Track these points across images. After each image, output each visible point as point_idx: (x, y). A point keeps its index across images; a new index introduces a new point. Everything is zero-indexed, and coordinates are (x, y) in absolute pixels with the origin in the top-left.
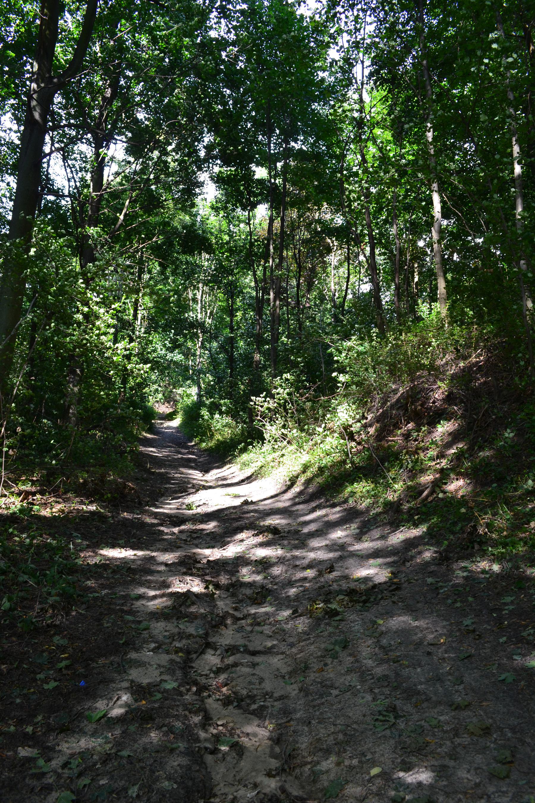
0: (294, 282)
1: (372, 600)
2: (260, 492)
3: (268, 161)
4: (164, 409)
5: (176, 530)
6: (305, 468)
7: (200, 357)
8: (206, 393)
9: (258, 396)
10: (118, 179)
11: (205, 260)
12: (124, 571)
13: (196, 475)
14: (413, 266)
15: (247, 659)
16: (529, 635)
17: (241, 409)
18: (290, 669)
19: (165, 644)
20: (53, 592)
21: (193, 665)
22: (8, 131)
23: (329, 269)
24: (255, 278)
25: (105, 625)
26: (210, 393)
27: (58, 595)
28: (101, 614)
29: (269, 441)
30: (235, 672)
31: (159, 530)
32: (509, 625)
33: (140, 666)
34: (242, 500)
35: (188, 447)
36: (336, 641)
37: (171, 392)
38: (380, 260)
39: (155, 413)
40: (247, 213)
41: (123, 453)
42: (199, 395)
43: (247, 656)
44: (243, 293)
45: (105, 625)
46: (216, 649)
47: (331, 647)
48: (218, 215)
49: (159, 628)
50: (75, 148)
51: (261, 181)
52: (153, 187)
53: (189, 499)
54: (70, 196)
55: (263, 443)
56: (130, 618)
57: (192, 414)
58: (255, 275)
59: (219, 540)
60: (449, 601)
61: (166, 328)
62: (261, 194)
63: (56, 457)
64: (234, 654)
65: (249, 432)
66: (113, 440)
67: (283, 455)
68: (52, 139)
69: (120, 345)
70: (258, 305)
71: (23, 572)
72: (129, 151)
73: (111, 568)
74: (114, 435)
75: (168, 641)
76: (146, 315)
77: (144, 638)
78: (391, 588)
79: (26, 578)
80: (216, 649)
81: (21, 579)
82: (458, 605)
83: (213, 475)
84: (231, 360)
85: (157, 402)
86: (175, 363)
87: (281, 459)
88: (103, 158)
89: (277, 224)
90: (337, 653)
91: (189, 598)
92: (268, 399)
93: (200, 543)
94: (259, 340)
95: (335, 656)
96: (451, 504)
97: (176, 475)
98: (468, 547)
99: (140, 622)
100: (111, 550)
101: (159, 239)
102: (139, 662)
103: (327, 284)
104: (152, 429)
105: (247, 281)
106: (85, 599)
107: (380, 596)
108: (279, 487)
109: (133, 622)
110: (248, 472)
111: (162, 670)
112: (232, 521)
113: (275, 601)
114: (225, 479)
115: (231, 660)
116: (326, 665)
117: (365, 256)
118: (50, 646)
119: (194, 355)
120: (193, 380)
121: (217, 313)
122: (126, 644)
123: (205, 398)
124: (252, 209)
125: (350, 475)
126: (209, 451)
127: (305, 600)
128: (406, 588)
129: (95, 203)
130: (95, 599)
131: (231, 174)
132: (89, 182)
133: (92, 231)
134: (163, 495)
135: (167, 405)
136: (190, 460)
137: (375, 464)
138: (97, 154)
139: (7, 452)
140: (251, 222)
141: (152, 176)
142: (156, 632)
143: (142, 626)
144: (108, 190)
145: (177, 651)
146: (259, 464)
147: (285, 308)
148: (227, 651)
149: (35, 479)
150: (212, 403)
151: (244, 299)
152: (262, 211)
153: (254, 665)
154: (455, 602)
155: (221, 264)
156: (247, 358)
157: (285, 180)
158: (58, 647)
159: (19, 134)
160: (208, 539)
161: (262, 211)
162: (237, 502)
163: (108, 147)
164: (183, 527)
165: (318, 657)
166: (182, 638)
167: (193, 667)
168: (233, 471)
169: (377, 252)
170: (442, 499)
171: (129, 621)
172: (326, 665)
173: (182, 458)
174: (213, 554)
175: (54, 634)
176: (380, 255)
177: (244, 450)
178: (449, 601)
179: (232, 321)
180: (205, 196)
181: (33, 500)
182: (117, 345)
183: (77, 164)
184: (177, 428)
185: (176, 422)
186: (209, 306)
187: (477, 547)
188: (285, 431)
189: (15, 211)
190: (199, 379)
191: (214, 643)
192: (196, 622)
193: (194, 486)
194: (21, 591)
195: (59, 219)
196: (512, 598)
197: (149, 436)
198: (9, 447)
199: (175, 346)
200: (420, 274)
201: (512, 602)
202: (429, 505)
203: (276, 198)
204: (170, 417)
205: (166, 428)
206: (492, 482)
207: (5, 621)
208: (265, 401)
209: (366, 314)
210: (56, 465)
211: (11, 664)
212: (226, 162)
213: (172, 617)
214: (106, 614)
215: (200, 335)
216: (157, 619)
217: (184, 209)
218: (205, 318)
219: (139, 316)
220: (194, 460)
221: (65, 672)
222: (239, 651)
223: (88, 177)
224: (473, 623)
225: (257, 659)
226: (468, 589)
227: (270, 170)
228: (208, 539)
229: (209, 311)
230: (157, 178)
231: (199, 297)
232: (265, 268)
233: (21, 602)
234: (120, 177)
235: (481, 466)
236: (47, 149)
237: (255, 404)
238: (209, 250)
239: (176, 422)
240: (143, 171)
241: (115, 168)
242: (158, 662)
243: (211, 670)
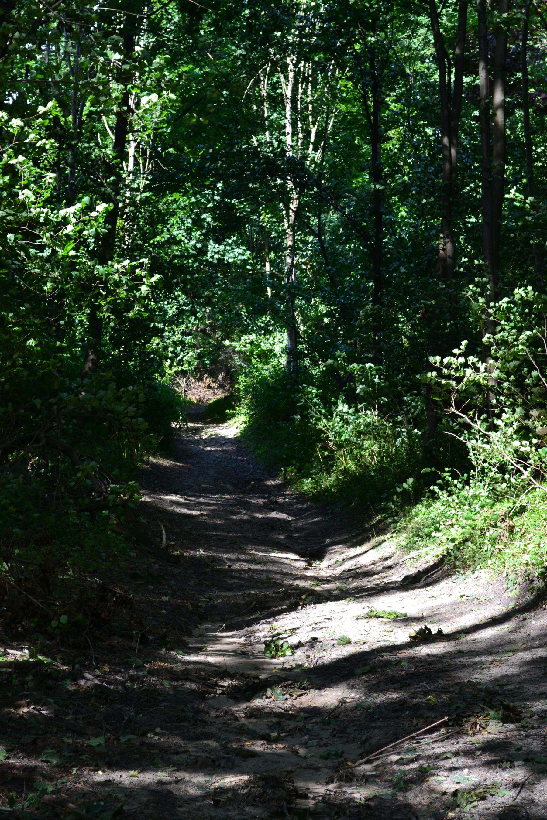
2: (471, 601)
4: (201, 391)
7: (293, 254)
8: (312, 347)
17: (405, 386)
24: (437, 36)
26: (321, 343)
37: (219, 347)
41: (94, 509)
42: (292, 352)
44: (406, 77)
53: (285, 622)
58: (434, 26)
61: (199, 177)
65: (426, 450)
67: (523, 509)
83: (334, 563)
85: (184, 373)
87: (517, 521)
92: (472, 359)
94: (451, 204)
97: (237, 566)
104: (170, 445)
105: (416, 43)
108: (513, 593)
110: (428, 555)
114: (369, 574)
119: (279, 248)
120: (276, 314)
121: (335, 133)
123: (307, 362)
126: (321, 500)
134: (203, 618)
135: (208, 381)
146: (457, 533)
147: (519, 113)
156: (419, 248)
162: (402, 635)
164: (258, 702)
168: (386, 552)
173: (252, 521)
177: (413, 498)
185: (232, 428)
186: (315, 113)
190: (291, 309)
197: (163, 462)
199: (228, 224)
204: (218, 413)
208: (466, 365)
218: (305, 146)
219: (131, 150)
228: (325, 734)
229: (314, 131)
237: (441, 375)
239: (232, 428)
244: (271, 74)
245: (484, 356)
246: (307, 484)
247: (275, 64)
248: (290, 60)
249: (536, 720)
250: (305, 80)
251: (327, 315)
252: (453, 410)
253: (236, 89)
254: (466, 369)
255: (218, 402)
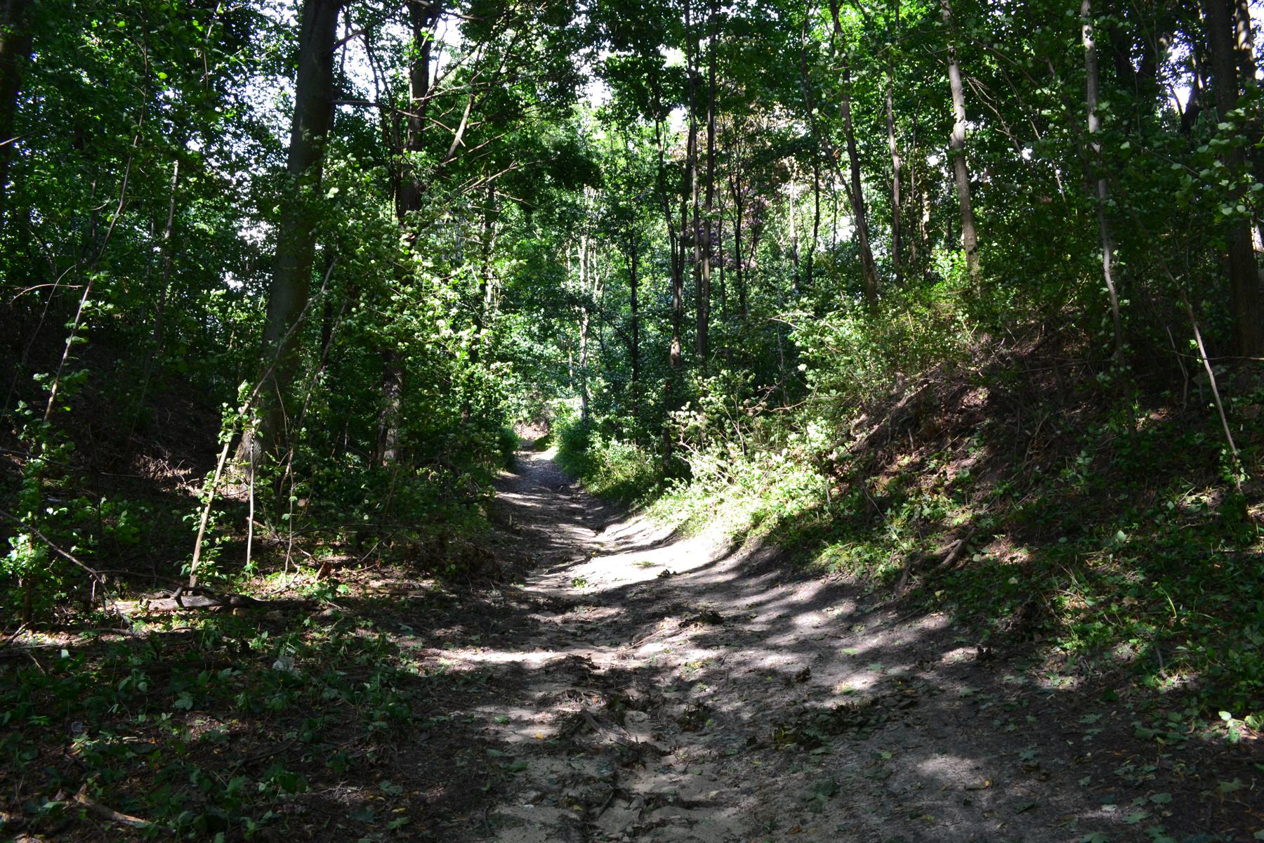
0: (729, 228)
1: (872, 721)
2: (681, 560)
3: (687, 38)
4: (530, 433)
5: (558, 619)
6: (757, 520)
8: (597, 406)
9: (677, 408)
10: (451, 77)
11: (589, 198)
12: (483, 682)
13: (585, 536)
14: (921, 197)
15: (679, 814)
16: (1126, 773)
17: (652, 429)
18: (747, 829)
19: (551, 792)
20: (377, 714)
21: (597, 824)
22: (278, 8)
23: (786, 205)
25: (459, 764)
26: (602, 407)
27: (383, 720)
28: (451, 746)
29: (699, 480)
30: (662, 834)
31: (533, 620)
32: (1095, 758)
33: (515, 825)
34: (659, 571)
35: (569, 492)
36: (819, 785)
38: (868, 190)
39: (517, 439)
40: (653, 124)
41: (469, 503)
42: (586, 411)
43: (679, 810)
45: (459, 764)
46: (630, 800)
47: (811, 795)
48: (609, 127)
49: (543, 768)
50: (383, 30)
51: (676, 71)
52: (506, 86)
53: (577, 572)
54: (378, 103)
55: (689, 485)
56: (494, 752)
57: (576, 440)
59: (620, 633)
60: (997, 723)
61: (531, 305)
62: (676, 90)
63: (368, 509)
64: (659, 807)
66: (455, 483)
67: (722, 500)
68: (347, 17)
69: (465, 334)
70: (676, 266)
71: (330, 685)
72: (468, 31)
73: (462, 677)
74: (456, 476)
75: (556, 787)
76: (499, 286)
77: (519, 783)
78: (903, 704)
79: (334, 693)
80: (630, 800)
81: (326, 695)
82: (1011, 727)
83: (613, 533)
84: (634, 353)
85: (520, 422)
86: (547, 360)
87: (718, 507)
88: (428, 43)
89: (702, 135)
90: (821, 804)
91: (585, 721)
92: (693, 413)
93: (598, 639)
95: (818, 810)
96: (993, 570)
98: (1023, 638)
99: (511, 759)
100: (460, 651)
101: (519, 166)
102: (513, 818)
103: (783, 230)
104: (511, 464)
106: (426, 725)
107: (885, 717)
109: (501, 758)
111: (549, 831)
112: (641, 607)
113: (719, 725)
115: (656, 817)
116: (804, 822)
117: (843, 182)
118: (376, 796)
120: (576, 387)
122: (492, 792)
123: (593, 415)
124: (662, 118)
125: (829, 530)
126: (600, 497)
127: (766, 723)
128: (926, 704)
129: (416, 115)
130: (441, 724)
131: (627, 62)
132: (407, 82)
133: (416, 156)
134: (534, 567)
135: (534, 426)
136: (574, 512)
137: (857, 517)
138: (419, 37)
139: (295, 503)
140: (662, 138)
141: (504, 70)
142: (536, 774)
143: (514, 765)
144: (437, 93)
145: (572, 802)
148: (647, 802)
149: (337, 543)
150: (607, 422)
151: (653, 256)
152: (678, 119)
153: (691, 824)
154: (1006, 723)
155: (615, 206)
157: (714, 68)
158: (388, 797)
159: (295, 12)
160: (609, 632)
161: (678, 119)
162: (652, 574)
163: (433, 24)
164: (569, 615)
165: (790, 810)
166: (577, 783)
167: (596, 827)
168: (642, 526)
169: (862, 177)
170: (979, 564)
171: (494, 758)
172: (804, 822)
174: (605, 659)
175: (381, 779)
176: (867, 180)
177: (658, 494)
178: (997, 723)
179: (634, 292)
180: (590, 99)
181: (338, 575)
182: (460, 333)
183: (386, 55)
184: (552, 462)
187: (1037, 637)
188: (723, 464)
189: (294, 131)
191: (628, 791)
192: (597, 758)
193: (581, 551)
194: (328, 713)
195: (362, 142)
196: (1098, 717)
198: (299, 496)
200: (933, 207)
201: (1098, 723)
202: (958, 574)
203: (701, 98)
204: (540, 445)
205: (534, 463)
206: (1059, 535)
207: (306, 758)
209: (850, 272)
210: (369, 521)
211: (319, 823)
212: (619, 44)
213: (560, 751)
214: (459, 748)
215: (586, 317)
216: (536, 754)
217: (555, 119)
219: (489, 289)
220: (581, 512)
221: (400, 834)
222: (666, 802)
223: (406, 72)
224: (1035, 756)
225: (695, 814)
226: (1025, 703)
227: (689, 53)
228: (609, 632)
230: (512, 70)
231: (581, 256)
232: (684, 210)
233: (329, 730)
234: (454, 72)
235: (1041, 510)
236: (340, 33)
237: (674, 422)
238: (596, 182)
239: (551, 453)
240: (490, 62)
241: (445, 58)
242: (542, 818)
243: (624, 831)
244: (572, 246)
245: (700, 411)
246: (594, 488)
247: (574, 240)
248: (583, 238)
249: (1194, 536)
250: (592, 249)
251: (606, 387)
252: (681, 443)
253: (552, 255)
254: (686, 419)
255: (540, 439)
